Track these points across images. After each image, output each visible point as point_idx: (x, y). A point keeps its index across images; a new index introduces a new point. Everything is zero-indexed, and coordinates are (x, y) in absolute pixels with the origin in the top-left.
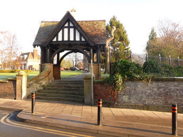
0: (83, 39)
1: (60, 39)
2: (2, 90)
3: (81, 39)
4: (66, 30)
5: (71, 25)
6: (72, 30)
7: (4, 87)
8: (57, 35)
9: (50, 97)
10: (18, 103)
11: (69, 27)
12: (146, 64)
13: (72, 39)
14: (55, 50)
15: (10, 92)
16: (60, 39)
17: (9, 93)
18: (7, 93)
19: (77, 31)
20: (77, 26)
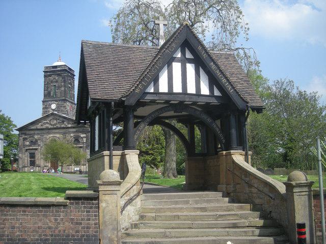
0: (217, 93)
1: (163, 87)
2: (50, 228)
3: (211, 90)
4: (177, 67)
5: (189, 55)
6: (190, 68)
7: (56, 220)
8: (156, 80)
9: (207, 230)
10: (299, 180)
11: (184, 61)
12: (263, 219)
13: (177, 88)
14: (90, 104)
15: (78, 231)
16: (163, 87)
17: (73, 236)
18: (68, 236)
19: (202, 72)
20: (201, 59)
